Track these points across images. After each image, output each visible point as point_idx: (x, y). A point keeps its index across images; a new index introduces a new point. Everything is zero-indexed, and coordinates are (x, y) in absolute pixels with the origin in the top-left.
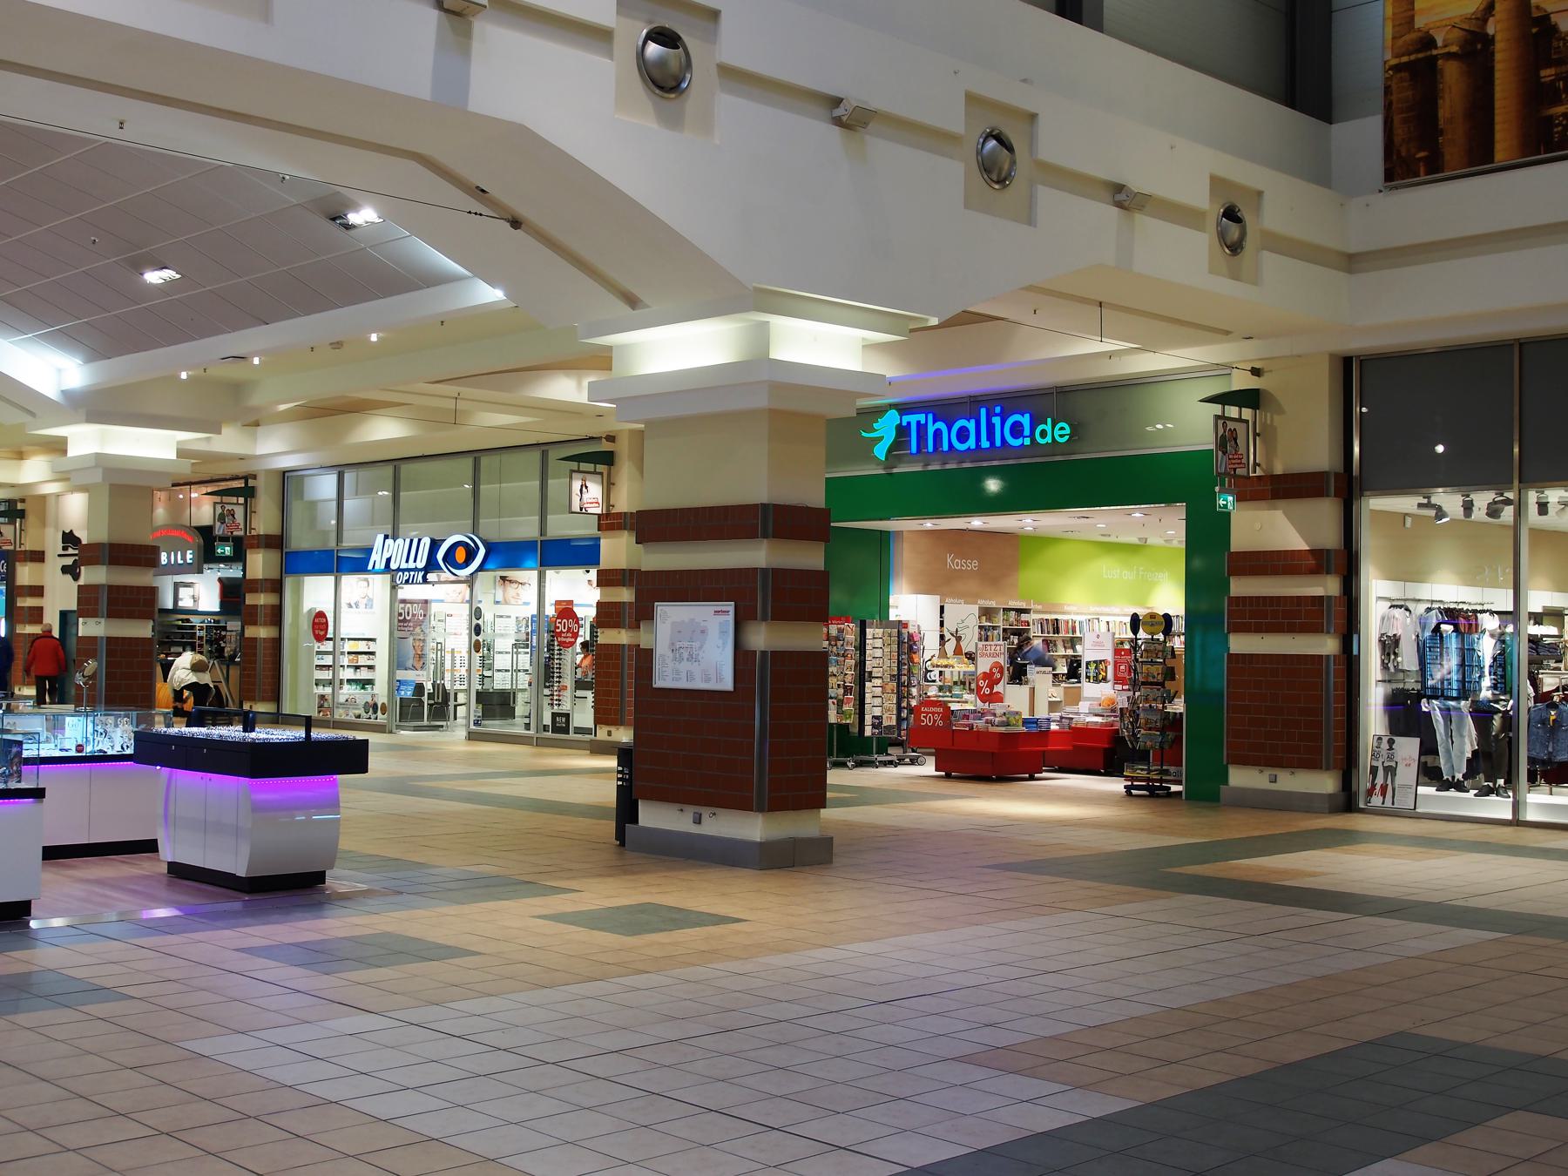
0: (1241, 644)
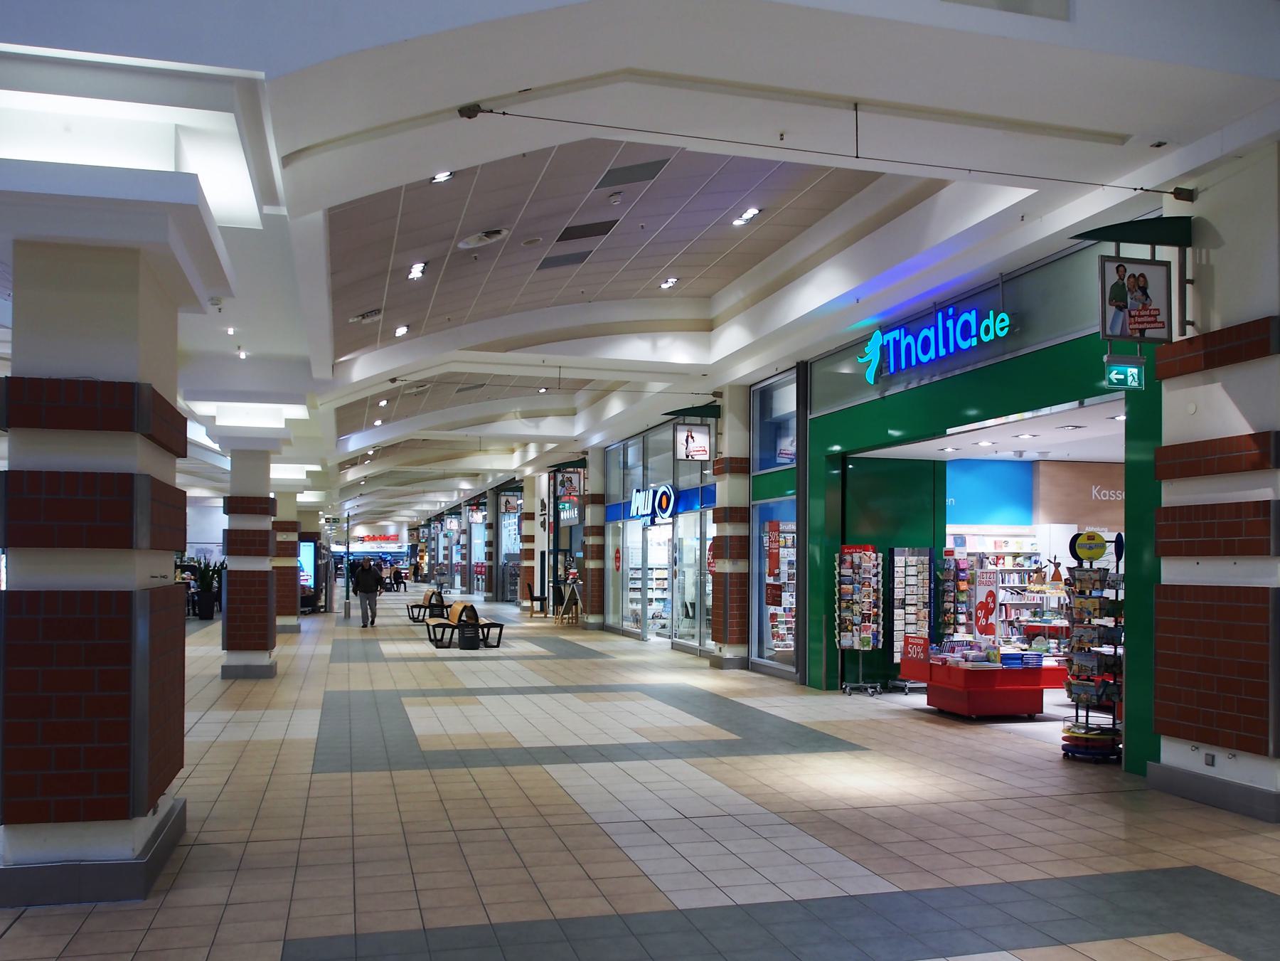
0: (1175, 572)
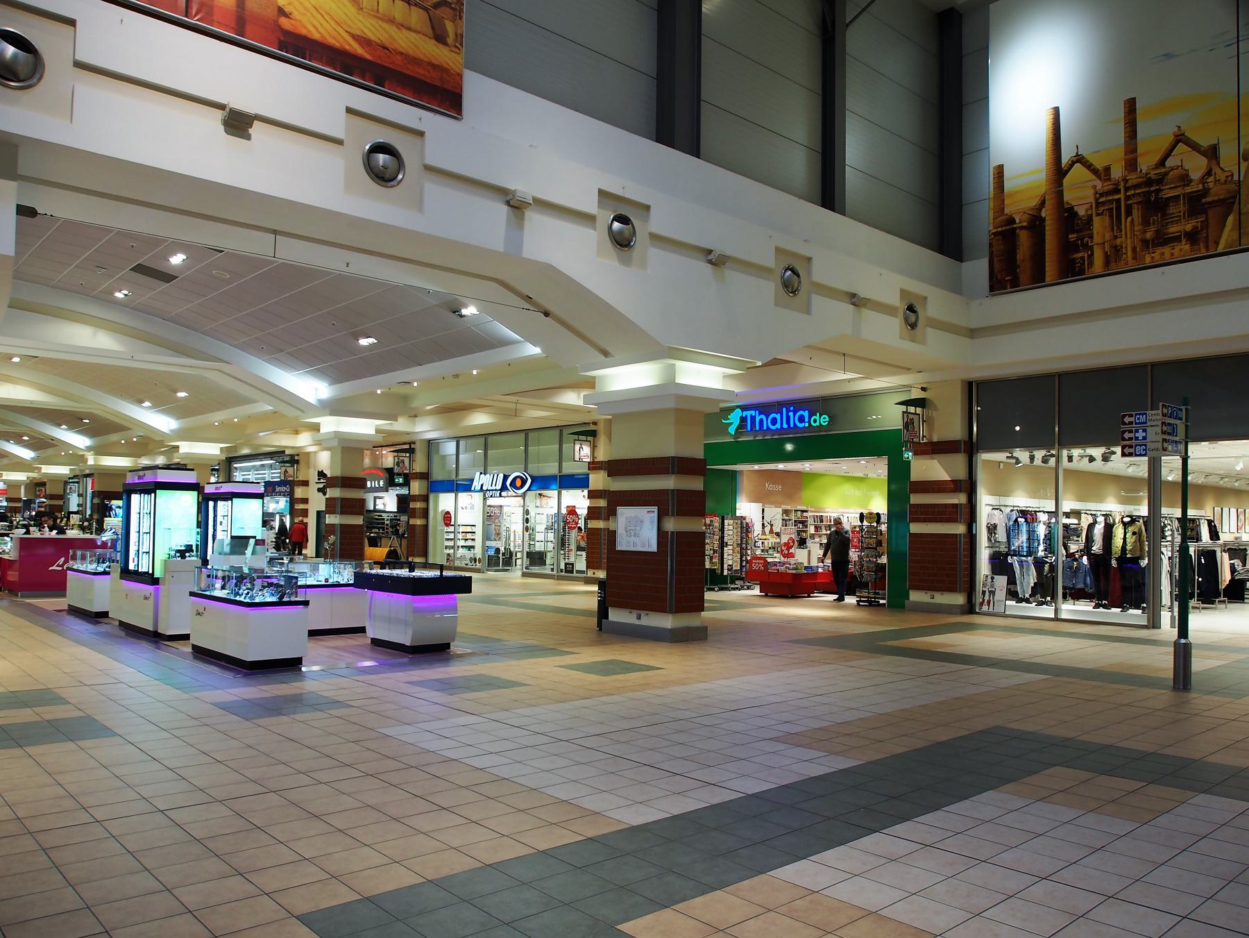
0: (915, 528)
